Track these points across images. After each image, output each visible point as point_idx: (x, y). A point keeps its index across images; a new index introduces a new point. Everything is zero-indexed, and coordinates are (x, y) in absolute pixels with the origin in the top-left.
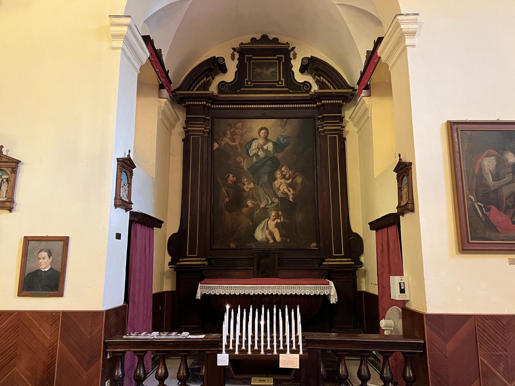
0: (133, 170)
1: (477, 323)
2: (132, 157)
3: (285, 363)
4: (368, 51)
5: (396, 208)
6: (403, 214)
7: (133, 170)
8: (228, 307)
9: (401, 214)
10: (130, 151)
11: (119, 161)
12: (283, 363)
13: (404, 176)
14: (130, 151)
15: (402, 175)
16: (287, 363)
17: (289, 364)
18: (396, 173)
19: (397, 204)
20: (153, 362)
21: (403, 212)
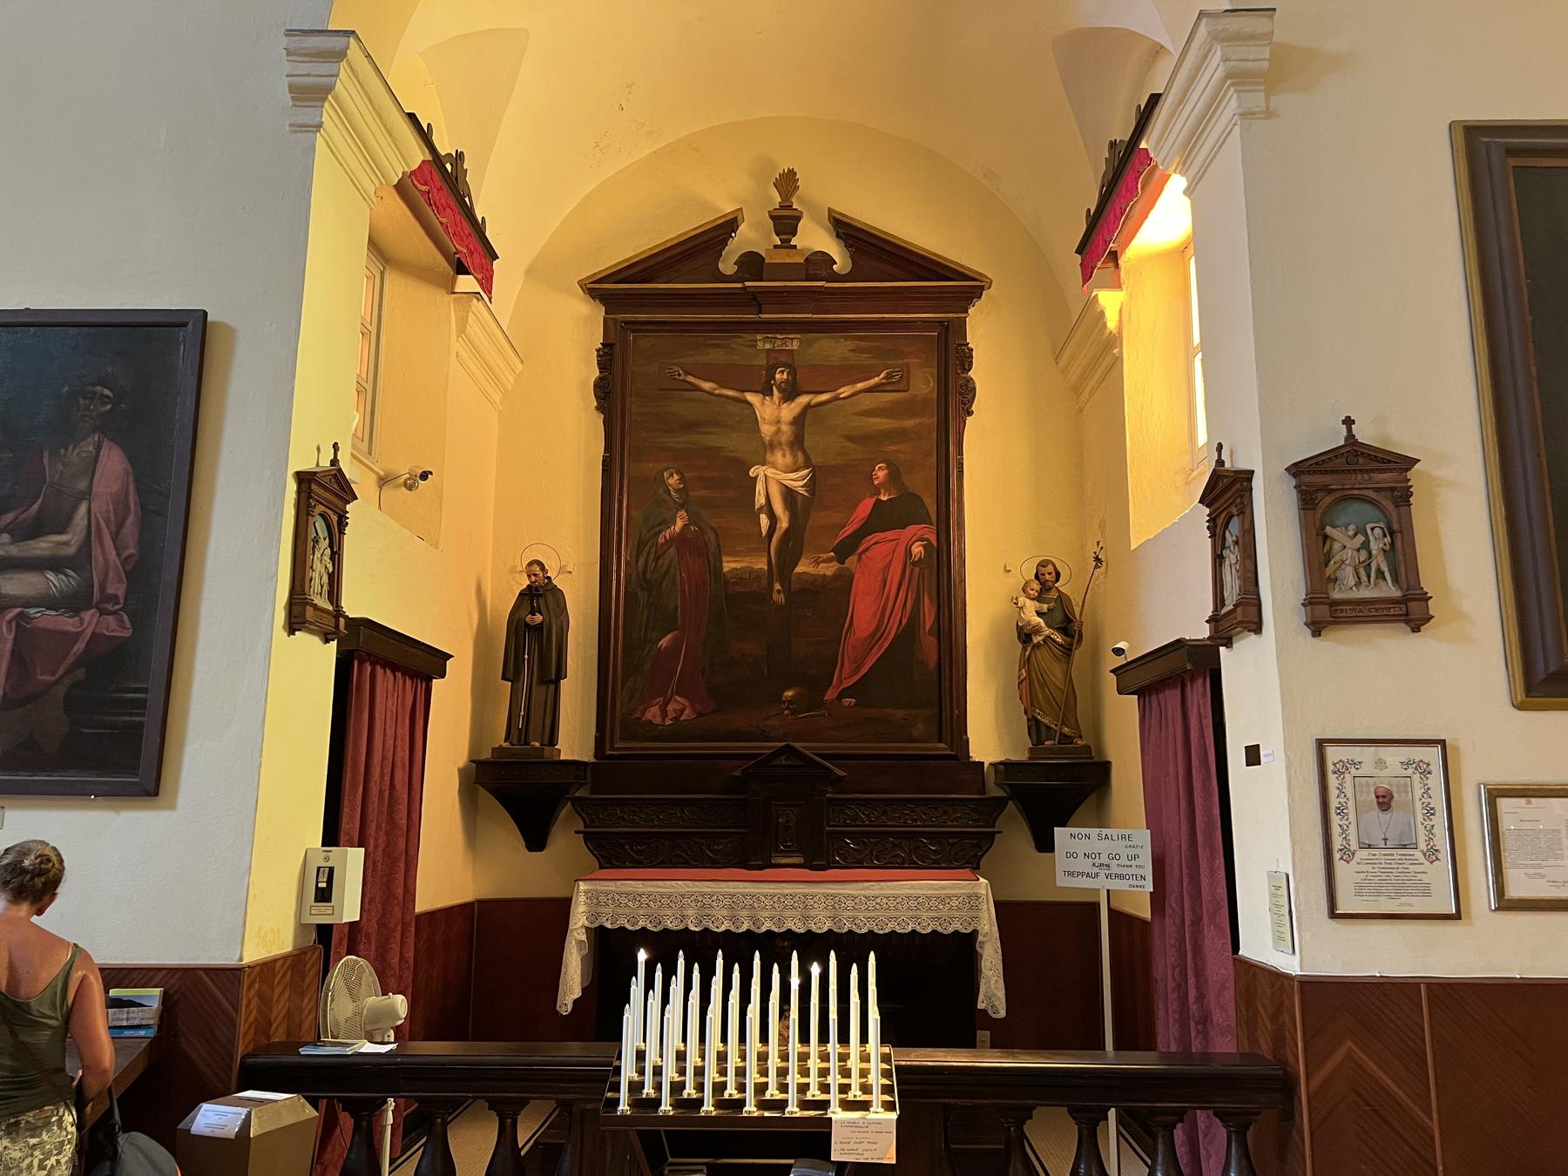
0: (348, 507)
1: (1431, 1119)
2: (346, 466)
3: (846, 1147)
4: (1113, 145)
5: (1207, 622)
6: (1229, 643)
7: (348, 507)
8: (642, 956)
9: (1224, 641)
10: (336, 447)
11: (303, 479)
12: (843, 1146)
13: (1233, 516)
14: (336, 447)
15: (1223, 516)
16: (855, 1146)
17: (860, 1151)
18: (1207, 507)
19: (1209, 612)
20: (407, 1140)
21: (1228, 634)
